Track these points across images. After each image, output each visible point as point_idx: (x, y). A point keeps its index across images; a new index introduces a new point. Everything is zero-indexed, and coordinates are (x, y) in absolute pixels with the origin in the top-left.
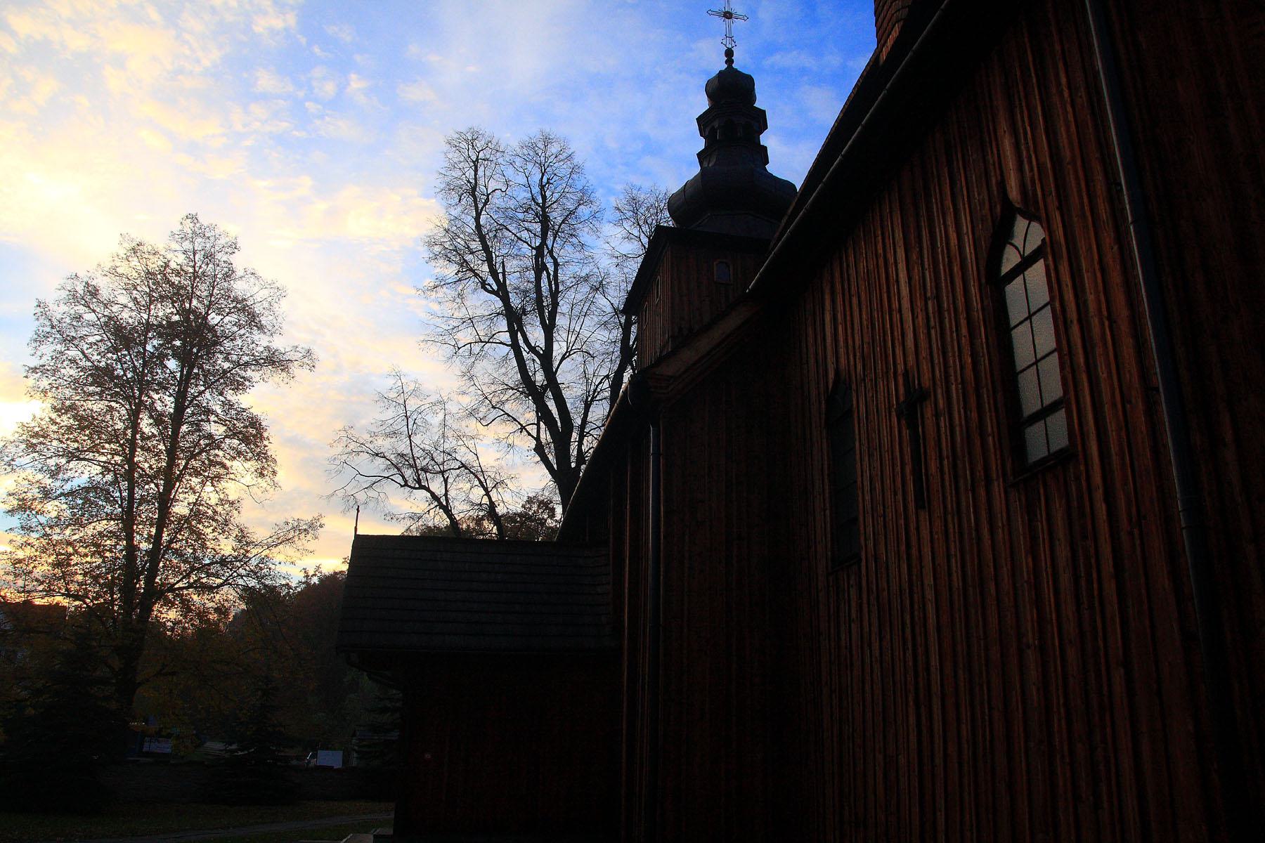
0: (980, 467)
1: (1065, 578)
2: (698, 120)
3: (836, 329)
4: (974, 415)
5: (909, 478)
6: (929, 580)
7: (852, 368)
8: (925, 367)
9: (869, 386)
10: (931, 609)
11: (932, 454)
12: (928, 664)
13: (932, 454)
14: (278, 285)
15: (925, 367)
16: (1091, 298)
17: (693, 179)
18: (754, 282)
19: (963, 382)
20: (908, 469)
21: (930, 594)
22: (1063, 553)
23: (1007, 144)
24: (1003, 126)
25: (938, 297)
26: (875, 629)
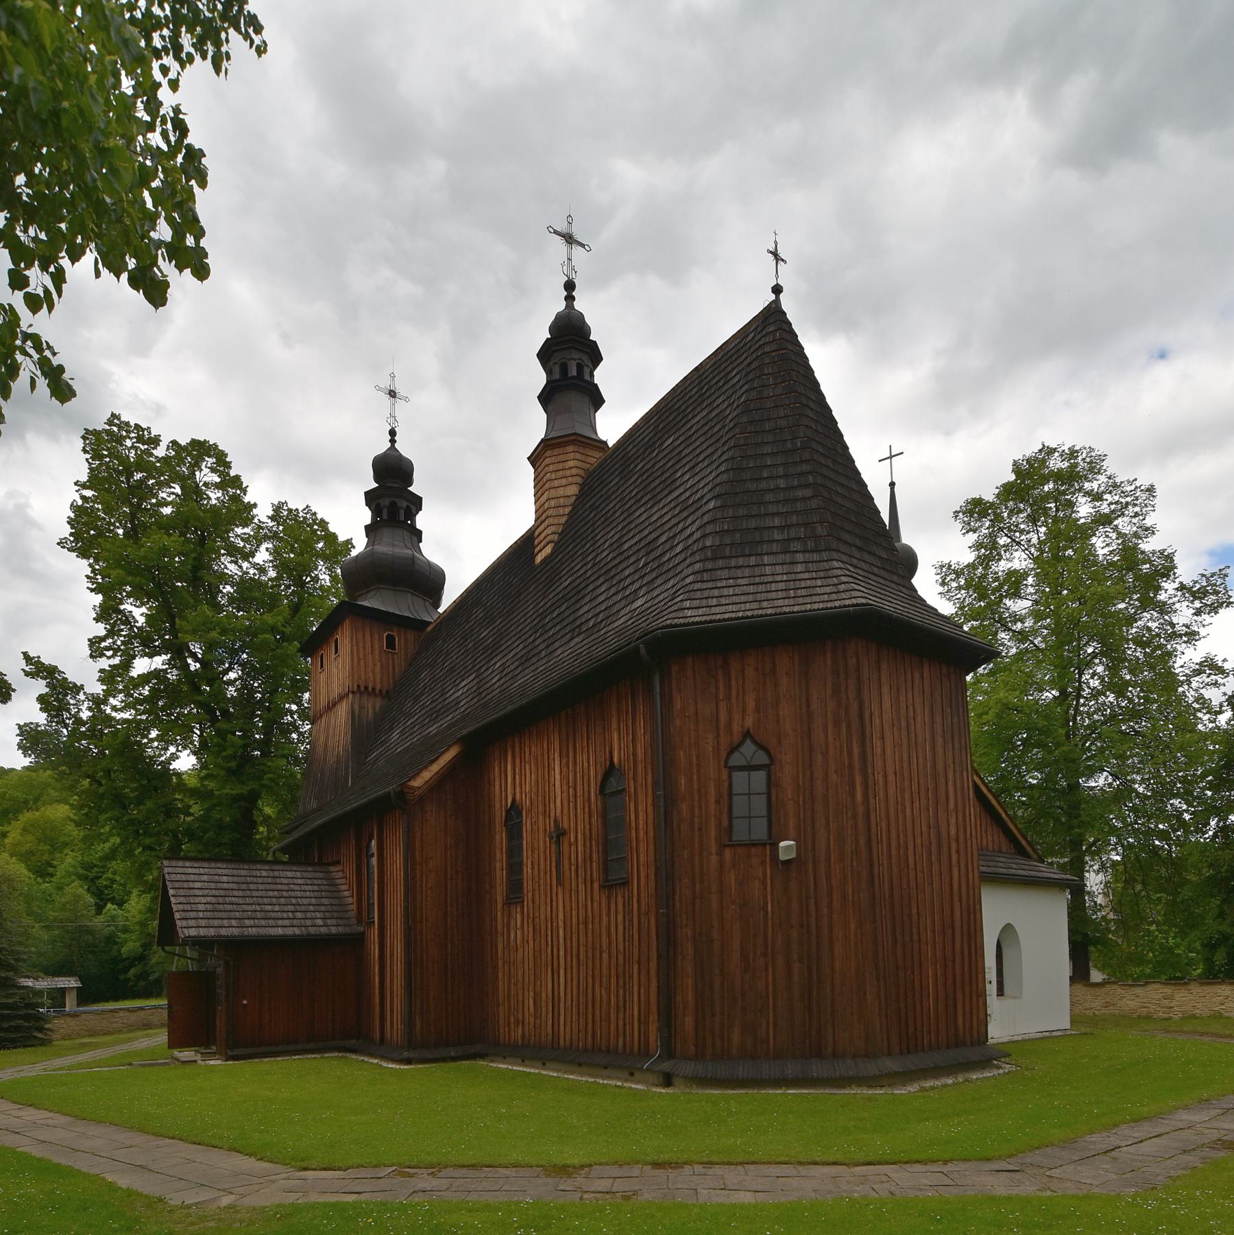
0: (589, 873)
1: (621, 928)
2: (604, 401)
3: (514, 779)
4: (588, 851)
5: (554, 869)
6: (561, 916)
7: (524, 802)
8: (565, 818)
9: (534, 814)
10: (561, 931)
11: (566, 863)
12: (558, 955)
13: (566, 863)
14: (941, 589)
15: (565, 818)
16: (641, 822)
17: (429, 564)
18: (435, 768)
19: (584, 834)
20: (554, 864)
21: (561, 924)
22: (620, 918)
23: (615, 735)
24: (614, 721)
25: (575, 789)
26: (531, 935)
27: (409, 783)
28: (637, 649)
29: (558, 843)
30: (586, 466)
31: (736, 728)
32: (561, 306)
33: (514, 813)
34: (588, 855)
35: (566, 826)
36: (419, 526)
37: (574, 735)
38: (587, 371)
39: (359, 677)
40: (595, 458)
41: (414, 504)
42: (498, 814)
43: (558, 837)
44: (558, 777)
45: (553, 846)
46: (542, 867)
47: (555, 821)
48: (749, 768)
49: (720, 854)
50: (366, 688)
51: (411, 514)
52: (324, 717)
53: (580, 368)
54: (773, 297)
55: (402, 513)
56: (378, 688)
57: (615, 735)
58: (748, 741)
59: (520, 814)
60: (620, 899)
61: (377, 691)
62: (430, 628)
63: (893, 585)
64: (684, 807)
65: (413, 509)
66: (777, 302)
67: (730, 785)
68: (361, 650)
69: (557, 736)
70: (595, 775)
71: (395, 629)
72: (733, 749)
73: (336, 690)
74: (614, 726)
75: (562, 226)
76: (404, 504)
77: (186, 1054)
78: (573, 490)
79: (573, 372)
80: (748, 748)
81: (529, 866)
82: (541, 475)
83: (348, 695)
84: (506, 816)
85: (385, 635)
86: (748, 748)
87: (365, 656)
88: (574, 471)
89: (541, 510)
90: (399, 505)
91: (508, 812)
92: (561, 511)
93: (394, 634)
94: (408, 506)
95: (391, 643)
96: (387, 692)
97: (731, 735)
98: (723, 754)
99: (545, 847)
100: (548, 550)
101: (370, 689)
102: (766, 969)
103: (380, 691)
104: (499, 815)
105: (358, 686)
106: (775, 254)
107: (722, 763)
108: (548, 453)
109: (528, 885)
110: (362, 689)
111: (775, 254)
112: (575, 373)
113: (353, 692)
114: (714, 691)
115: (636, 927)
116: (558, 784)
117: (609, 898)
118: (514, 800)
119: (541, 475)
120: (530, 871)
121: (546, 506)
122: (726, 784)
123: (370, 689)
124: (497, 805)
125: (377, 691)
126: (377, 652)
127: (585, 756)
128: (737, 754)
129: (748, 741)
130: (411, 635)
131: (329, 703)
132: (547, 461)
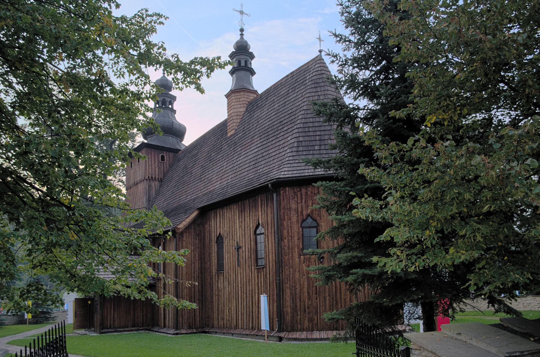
4: (250, 254)
20: (236, 259)
25: (245, 231)
27: (177, 227)
28: (268, 185)
29: (238, 251)
30: (249, 100)
31: (304, 213)
32: (238, 38)
33: (220, 239)
34: (250, 256)
35: (241, 245)
36: (175, 108)
37: (244, 211)
38: (248, 63)
39: (149, 174)
40: (252, 97)
41: (172, 99)
42: (213, 238)
43: (238, 249)
44: (238, 226)
45: (236, 252)
46: (231, 260)
47: (237, 243)
48: (310, 227)
49: (299, 258)
50: (152, 177)
51: (171, 103)
52: (132, 188)
53: (246, 62)
54: (319, 53)
55: (168, 103)
56: (157, 177)
57: (260, 212)
58: (309, 218)
59: (222, 239)
60: (262, 273)
61: (157, 179)
62: (180, 152)
63: (254, 299)
64: (286, 241)
65: (172, 101)
66: (320, 55)
67: (303, 234)
68: (150, 162)
69: (237, 211)
70: (252, 226)
71: (165, 152)
72: (304, 221)
73: (139, 178)
74: (260, 209)
75: (239, 9)
76: (169, 100)
77: (82, 331)
78: (243, 109)
79: (243, 64)
80: (310, 220)
81: (227, 259)
82: (231, 102)
83: (144, 180)
84: (217, 239)
85: (160, 155)
86: (310, 220)
87: (151, 164)
88: (244, 102)
89: (230, 116)
90: (166, 100)
91: (217, 238)
92: (238, 117)
93: (165, 155)
94: (170, 101)
95: (163, 158)
96: (161, 179)
97: (303, 216)
98: (300, 222)
99: (233, 252)
100: (233, 132)
101: (154, 178)
102: (317, 299)
103: (158, 178)
104: (214, 239)
105: (149, 177)
106: (320, 39)
107: (300, 225)
108: (233, 95)
109: (226, 267)
110: (150, 178)
111: (320, 39)
112: (244, 65)
113: (146, 180)
114: (296, 200)
115: (268, 284)
116: (238, 229)
117: (258, 273)
118: (220, 234)
119: (231, 102)
120: (227, 261)
121: (232, 115)
122: (301, 233)
123: (154, 178)
124: (213, 235)
125: (157, 179)
126: (157, 163)
127: (249, 219)
128: (305, 222)
129: (309, 218)
130: (171, 154)
131: (134, 183)
132: (233, 98)
